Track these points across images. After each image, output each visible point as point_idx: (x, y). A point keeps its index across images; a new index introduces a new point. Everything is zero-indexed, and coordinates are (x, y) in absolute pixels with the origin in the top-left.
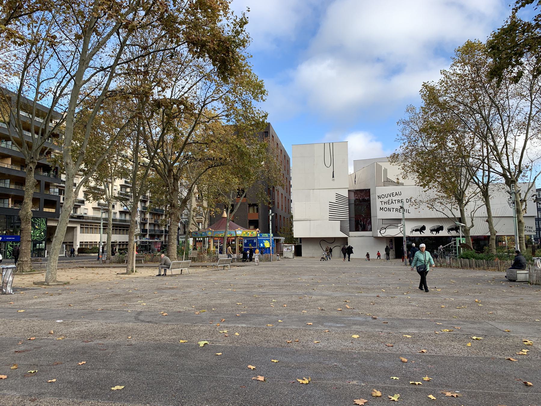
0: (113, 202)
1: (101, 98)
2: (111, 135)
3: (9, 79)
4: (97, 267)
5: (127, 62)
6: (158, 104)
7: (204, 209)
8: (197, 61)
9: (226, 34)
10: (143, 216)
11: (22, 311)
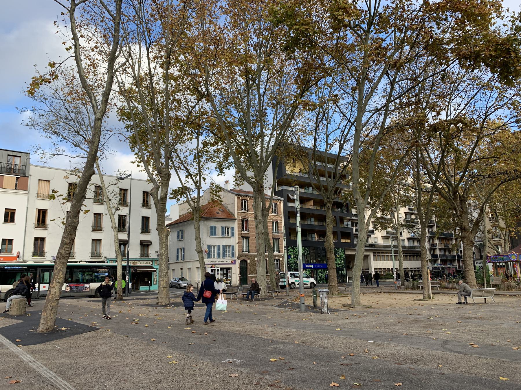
0: (401, 229)
1: (380, 136)
2: (391, 168)
3: (306, 138)
4: (393, 293)
5: (399, 97)
6: (434, 128)
7: (502, 229)
8: (472, 74)
9: (504, 35)
10: (431, 242)
11: (339, 329)
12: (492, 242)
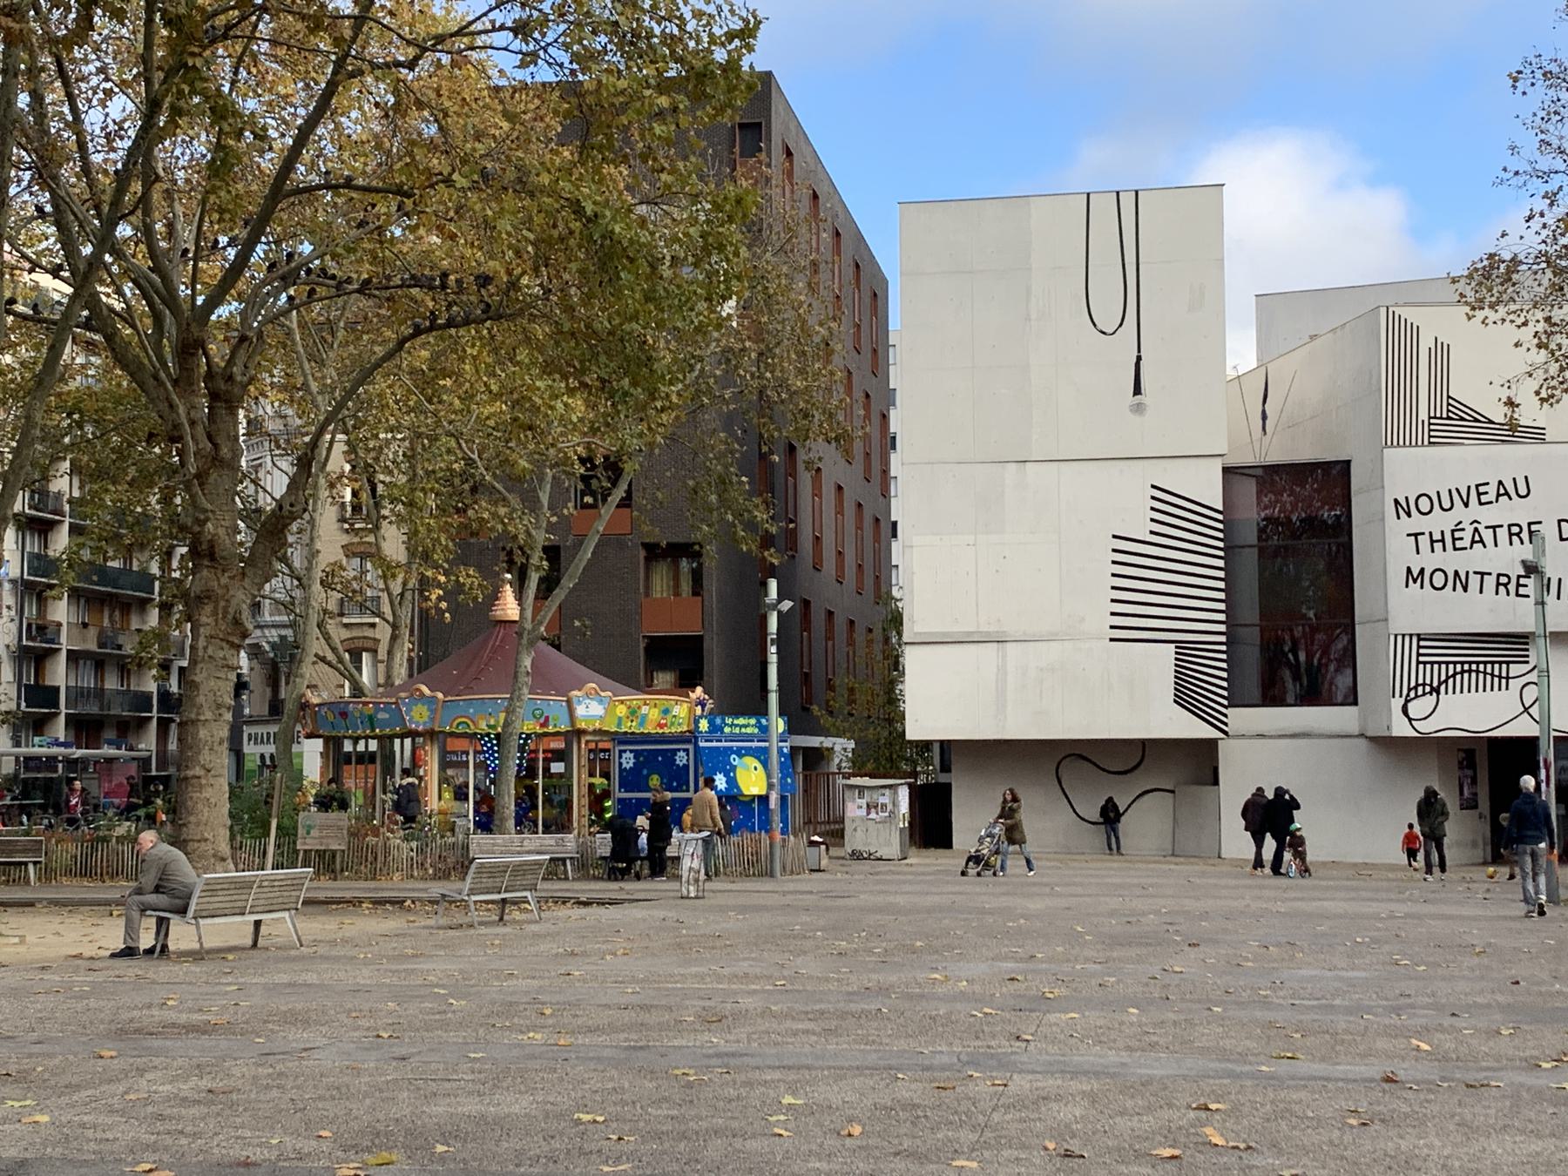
7: (388, 570)
10: (31, 610)
12: (338, 634)
